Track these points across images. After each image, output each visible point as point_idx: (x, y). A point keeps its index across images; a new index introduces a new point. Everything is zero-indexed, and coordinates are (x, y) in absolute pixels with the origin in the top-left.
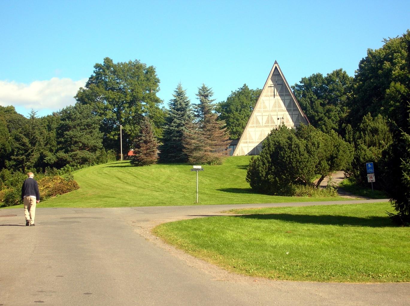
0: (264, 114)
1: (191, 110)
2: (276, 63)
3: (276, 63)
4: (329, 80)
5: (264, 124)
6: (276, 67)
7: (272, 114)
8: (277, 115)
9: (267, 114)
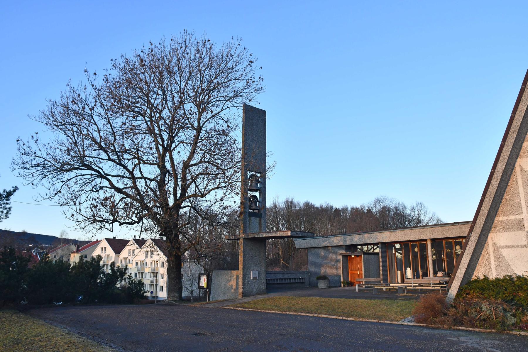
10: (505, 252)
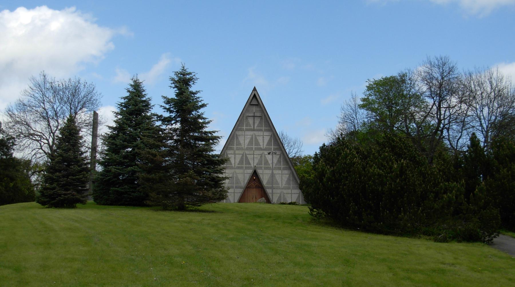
0: (237, 152)
1: (158, 108)
2: (255, 89)
3: (255, 89)
4: (390, 78)
5: (236, 165)
6: (255, 94)
7: (247, 152)
8: (254, 154)
9: (241, 152)
10: (285, 195)
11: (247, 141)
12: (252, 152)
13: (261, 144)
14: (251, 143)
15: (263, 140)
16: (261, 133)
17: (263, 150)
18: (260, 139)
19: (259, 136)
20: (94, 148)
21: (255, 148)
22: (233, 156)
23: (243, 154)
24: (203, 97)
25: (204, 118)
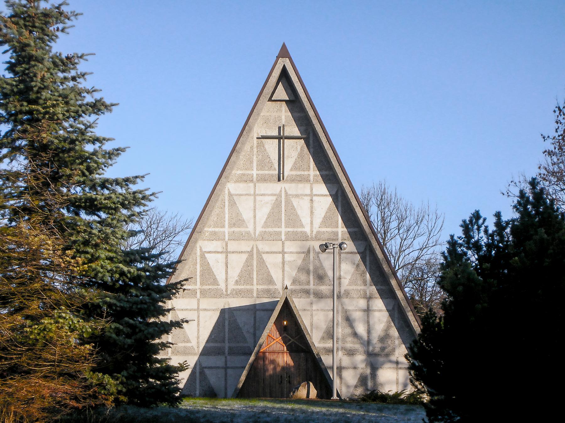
0: (233, 246)
7: (263, 246)
8: (283, 253)
9: (245, 246)
11: (263, 213)
12: (277, 246)
13: (305, 219)
14: (274, 218)
15: (312, 207)
16: (305, 188)
17: (256, 240)
18: (302, 208)
19: (297, 196)
20: (133, 234)
21: (287, 233)
22: (221, 257)
23: (251, 253)
24: (96, 78)
25: (95, 140)
